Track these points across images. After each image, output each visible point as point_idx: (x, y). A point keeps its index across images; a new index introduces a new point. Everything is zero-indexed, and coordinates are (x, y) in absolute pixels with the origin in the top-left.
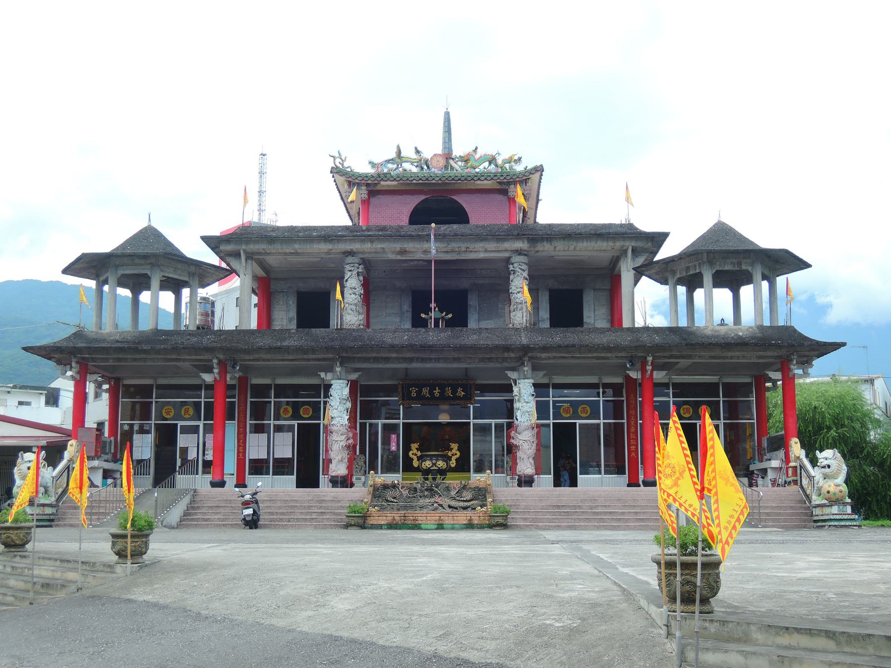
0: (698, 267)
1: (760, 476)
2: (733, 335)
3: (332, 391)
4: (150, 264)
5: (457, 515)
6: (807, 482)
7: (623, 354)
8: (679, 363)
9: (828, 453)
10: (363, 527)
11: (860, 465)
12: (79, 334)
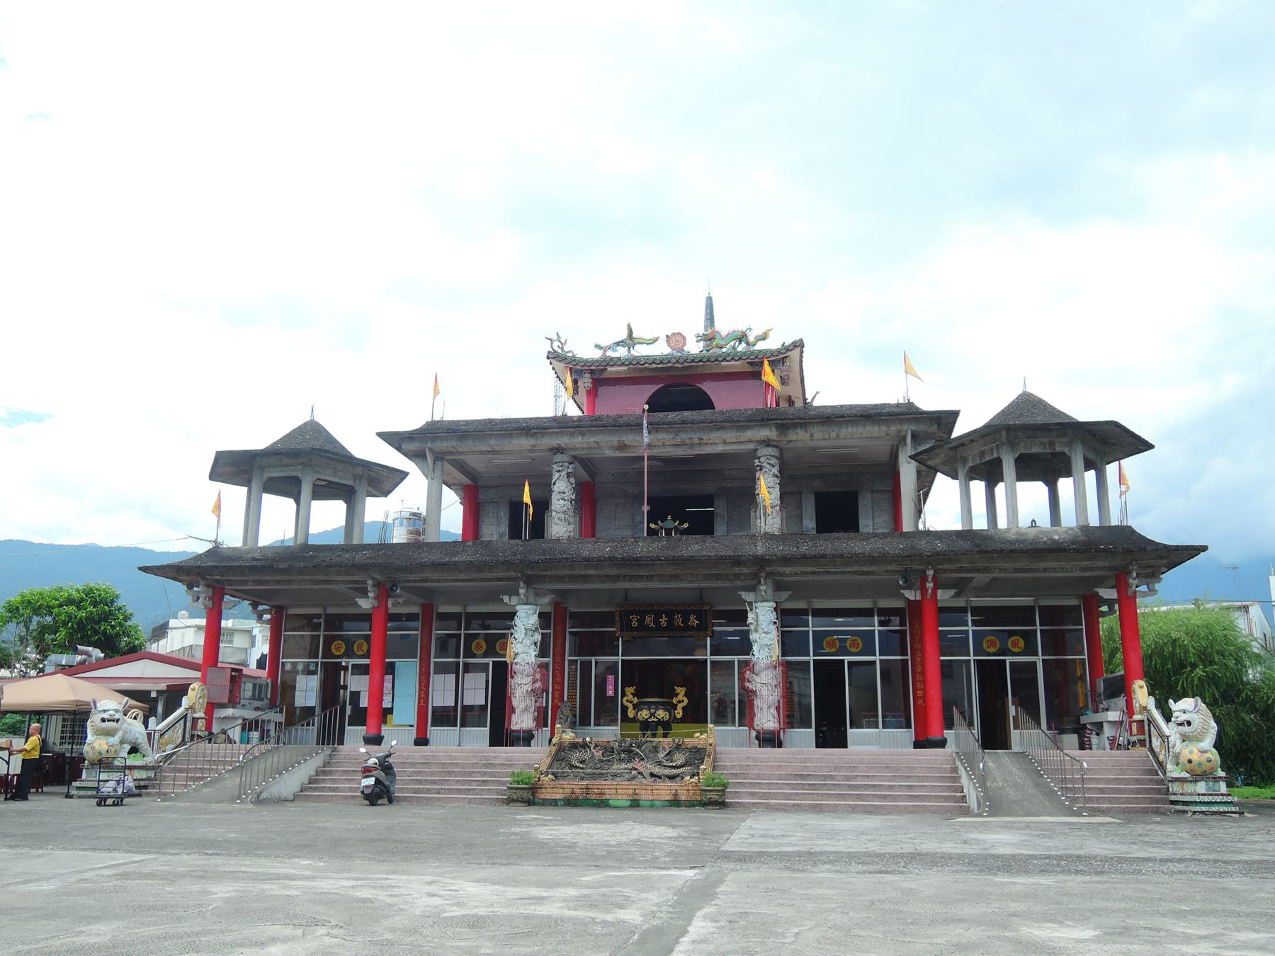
0: (995, 451)
1: (1094, 733)
2: (1045, 539)
3: (517, 621)
4: (301, 464)
5: (657, 787)
6: (1159, 744)
7: (893, 567)
8: (973, 578)
9: (1187, 703)
10: (530, 803)
11: (1236, 711)
12: (215, 551)
